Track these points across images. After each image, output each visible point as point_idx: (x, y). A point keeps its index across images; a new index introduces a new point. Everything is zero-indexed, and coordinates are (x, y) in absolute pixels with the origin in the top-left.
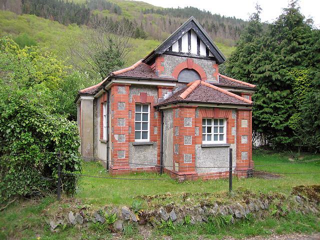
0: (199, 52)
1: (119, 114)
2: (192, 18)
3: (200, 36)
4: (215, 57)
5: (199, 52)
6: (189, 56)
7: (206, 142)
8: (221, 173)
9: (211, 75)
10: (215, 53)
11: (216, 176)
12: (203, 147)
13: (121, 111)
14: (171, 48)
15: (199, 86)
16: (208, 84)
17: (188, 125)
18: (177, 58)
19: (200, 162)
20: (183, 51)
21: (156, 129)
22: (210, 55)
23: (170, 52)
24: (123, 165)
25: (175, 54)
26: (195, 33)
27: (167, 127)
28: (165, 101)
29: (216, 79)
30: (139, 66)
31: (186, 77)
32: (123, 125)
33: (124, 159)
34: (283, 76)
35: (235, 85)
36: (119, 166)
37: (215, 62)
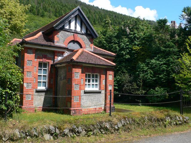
0: (76, 28)
1: (28, 69)
2: (78, 7)
3: (83, 19)
4: (91, 35)
5: (76, 28)
6: (76, 32)
7: (87, 89)
8: (96, 109)
9: (89, 48)
10: (92, 32)
11: (93, 111)
12: (86, 92)
13: (29, 67)
14: (64, 26)
15: (82, 53)
16: (88, 52)
17: (77, 77)
18: (67, 33)
19: (83, 102)
20: (71, 28)
21: (52, 80)
22: (88, 32)
23: (63, 29)
24: (29, 105)
25: (67, 30)
26: (80, 17)
27: (61, 79)
28: (59, 61)
29: (92, 49)
30: (41, 36)
31: (75, 46)
32: (30, 76)
33: (30, 101)
34: (185, 75)
35: (104, 53)
36: (26, 105)
37: (91, 37)
